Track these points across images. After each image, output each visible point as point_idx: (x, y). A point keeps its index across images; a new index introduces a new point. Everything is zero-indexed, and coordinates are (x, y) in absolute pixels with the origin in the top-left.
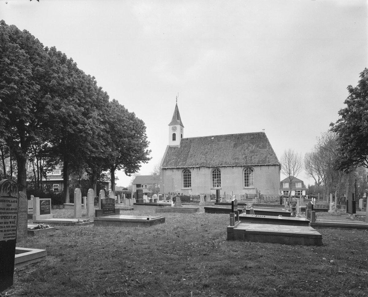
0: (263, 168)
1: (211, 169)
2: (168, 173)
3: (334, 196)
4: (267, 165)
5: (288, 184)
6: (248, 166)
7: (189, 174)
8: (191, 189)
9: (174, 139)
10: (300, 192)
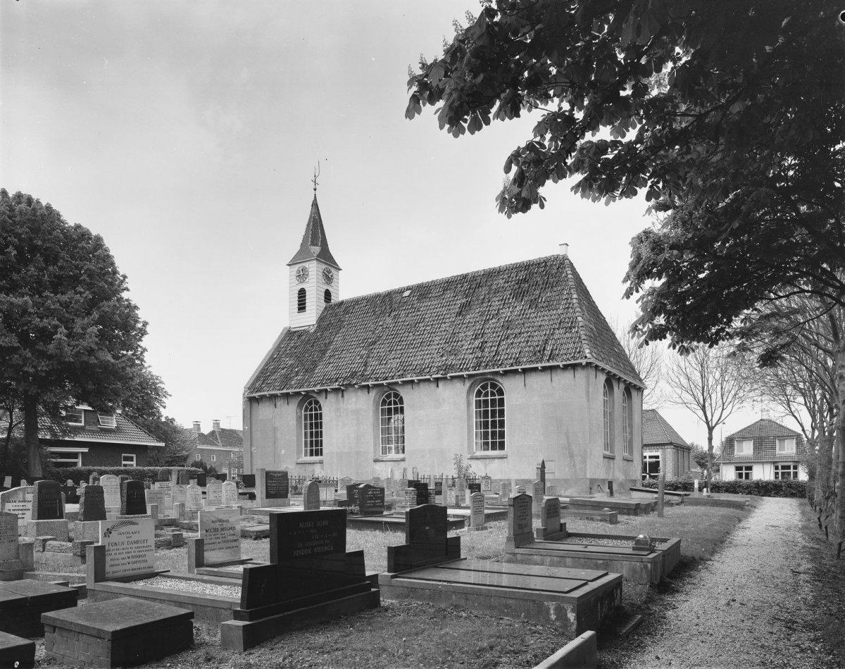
0: (533, 379)
1: (373, 393)
2: (264, 411)
3: (337, 503)
4: (544, 369)
5: (752, 443)
6: (481, 374)
7: (319, 412)
8: (321, 462)
9: (302, 307)
10: (789, 467)
